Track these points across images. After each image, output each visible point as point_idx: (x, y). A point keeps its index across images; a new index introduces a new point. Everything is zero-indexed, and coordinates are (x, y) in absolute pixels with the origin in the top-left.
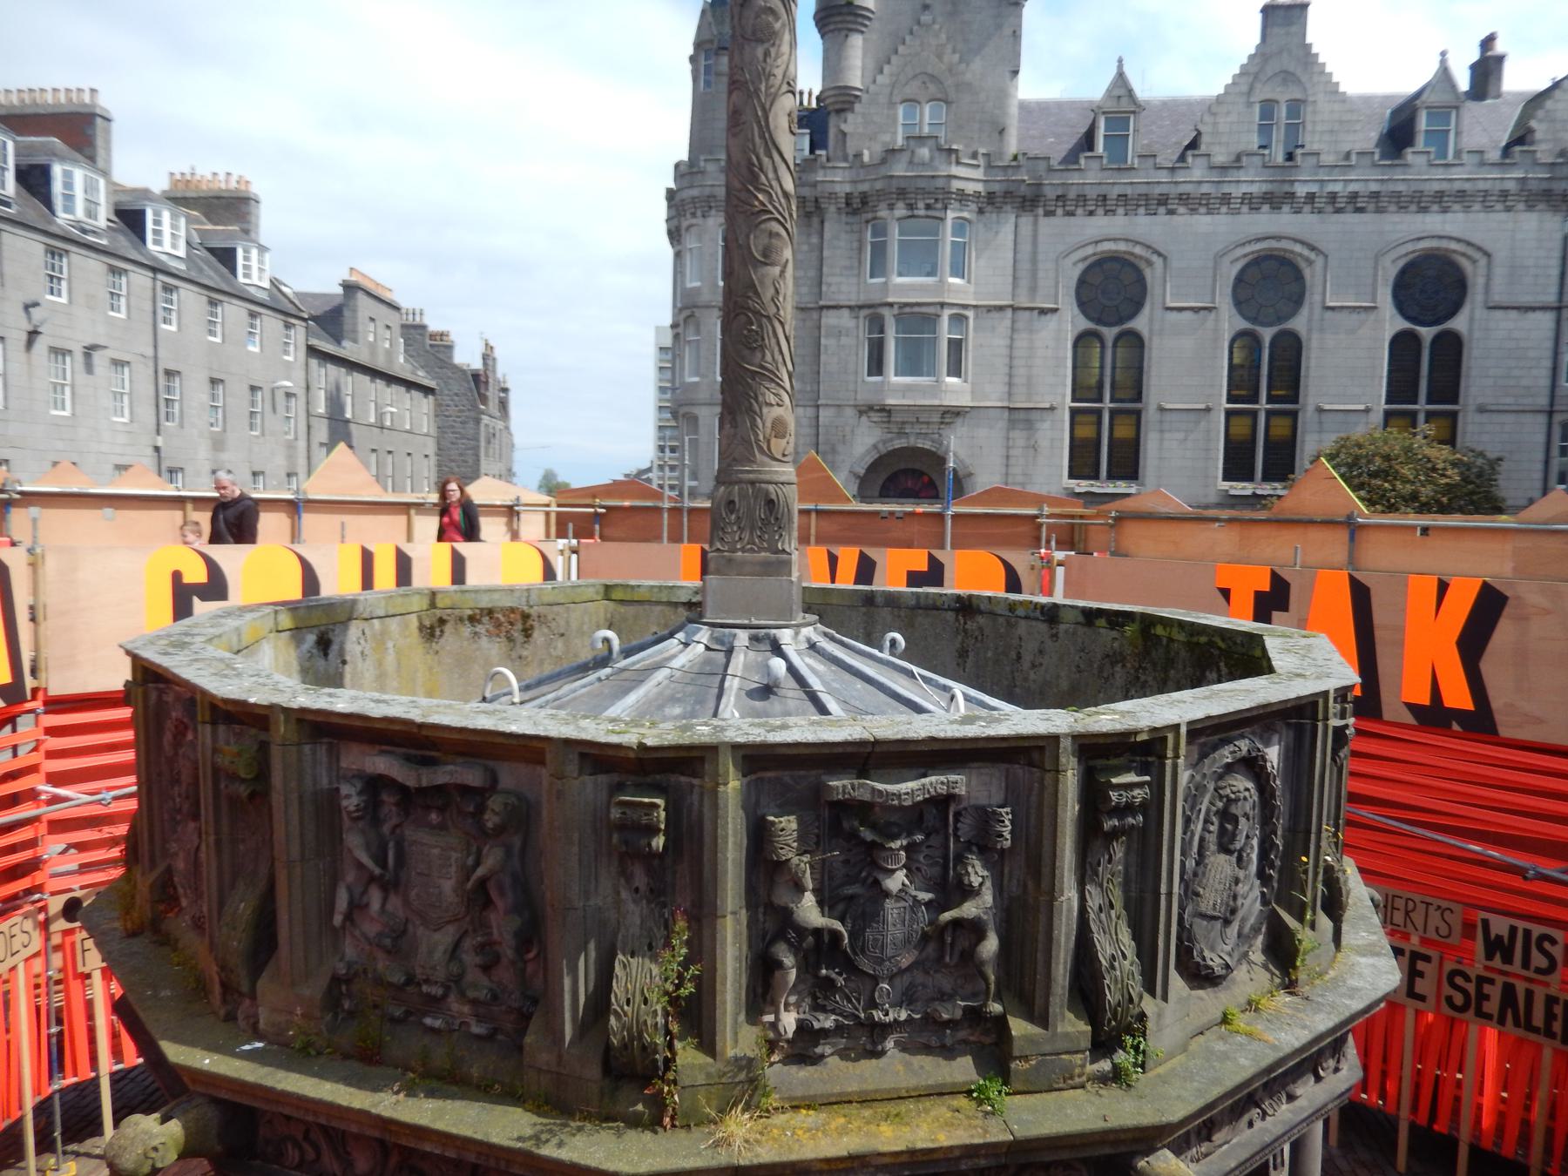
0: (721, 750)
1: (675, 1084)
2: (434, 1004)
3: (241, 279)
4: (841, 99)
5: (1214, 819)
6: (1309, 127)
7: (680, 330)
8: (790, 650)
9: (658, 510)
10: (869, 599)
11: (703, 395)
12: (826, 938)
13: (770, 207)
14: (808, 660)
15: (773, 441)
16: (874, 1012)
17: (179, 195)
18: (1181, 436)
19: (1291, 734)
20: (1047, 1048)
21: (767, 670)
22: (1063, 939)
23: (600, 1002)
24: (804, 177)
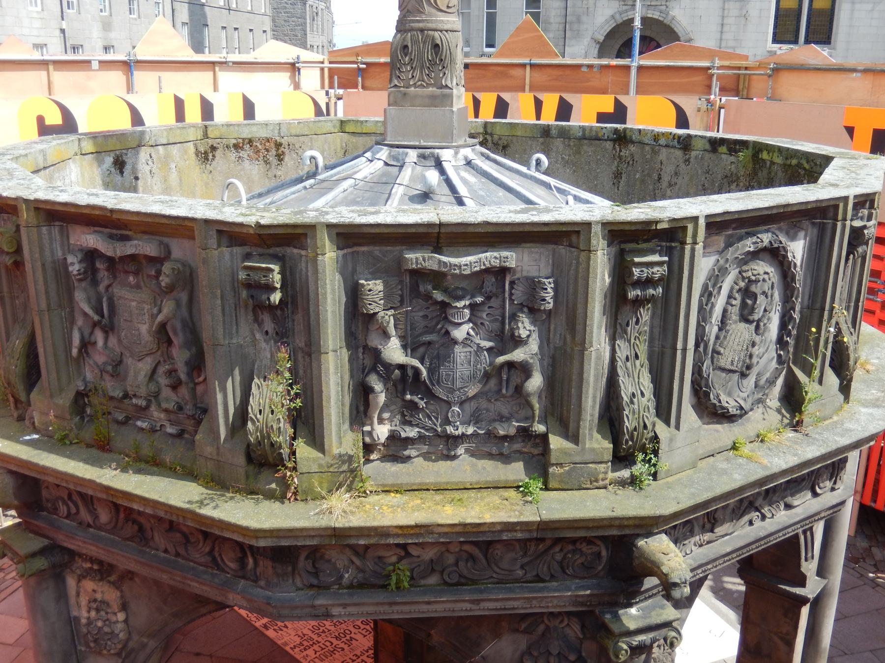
0: (318, 227)
2: (142, 411)
10: (564, 133)
12: (410, 373)
16: (447, 428)
18: (869, 7)
19: (815, 231)
20: (578, 459)
21: (424, 178)
22: (592, 380)
23: (242, 414)
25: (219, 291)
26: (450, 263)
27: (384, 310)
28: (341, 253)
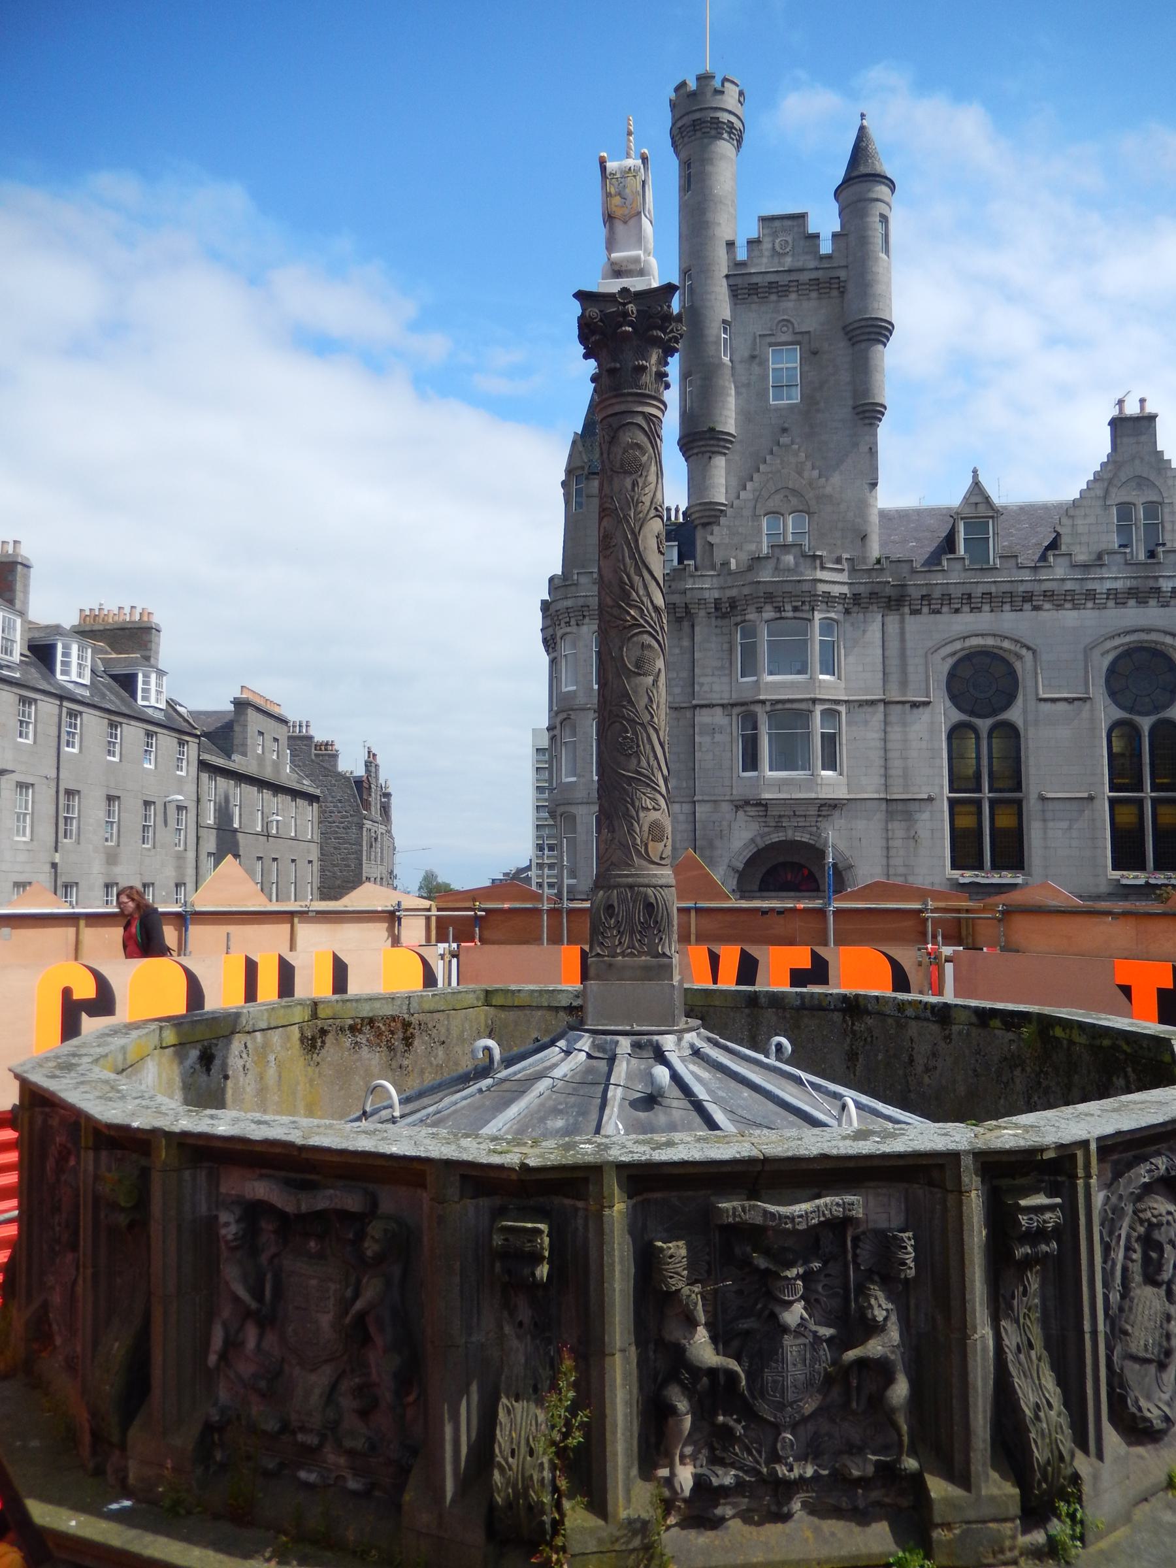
0: (606, 1169)
1: (565, 1552)
2: (309, 1455)
3: (140, 702)
4: (707, 513)
5: (1136, 1246)
6: (1168, 526)
7: (557, 732)
8: (673, 1057)
9: (537, 911)
10: (753, 1000)
11: (580, 794)
13: (642, 621)
14: (692, 1067)
15: (651, 844)
16: (778, 1467)
17: (87, 629)
18: (1065, 825)
20: (971, 1514)
21: (650, 1078)
22: (980, 1383)
24: (674, 585)
25: (458, 1263)
26: (779, 1214)
27: (688, 1285)
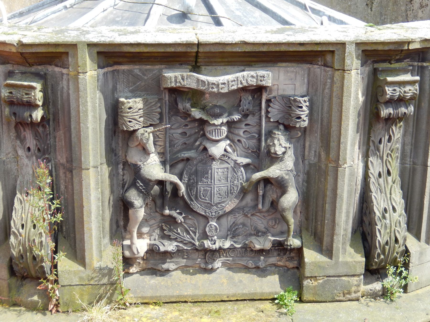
16: (205, 242)
20: (331, 272)
26: (208, 82)
27: (144, 127)
28: (102, 71)
